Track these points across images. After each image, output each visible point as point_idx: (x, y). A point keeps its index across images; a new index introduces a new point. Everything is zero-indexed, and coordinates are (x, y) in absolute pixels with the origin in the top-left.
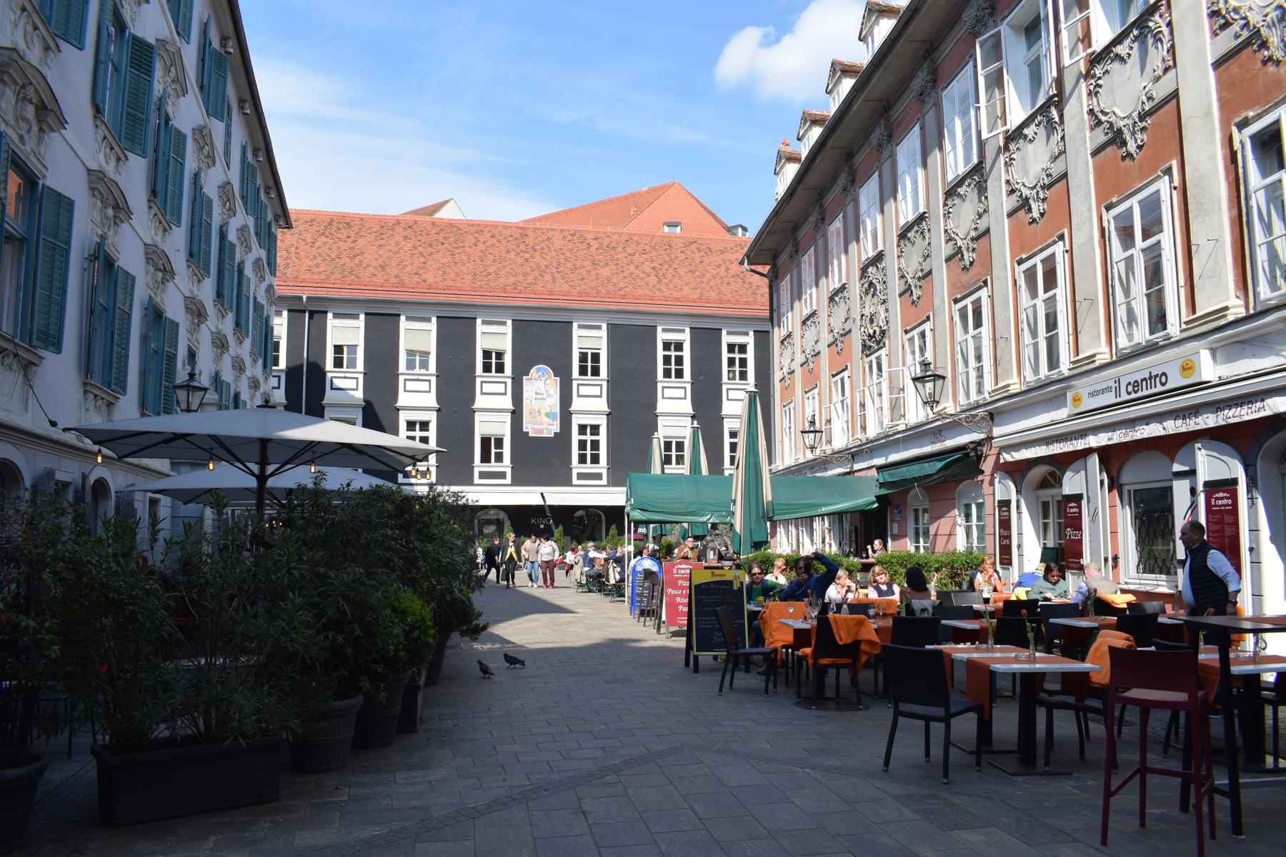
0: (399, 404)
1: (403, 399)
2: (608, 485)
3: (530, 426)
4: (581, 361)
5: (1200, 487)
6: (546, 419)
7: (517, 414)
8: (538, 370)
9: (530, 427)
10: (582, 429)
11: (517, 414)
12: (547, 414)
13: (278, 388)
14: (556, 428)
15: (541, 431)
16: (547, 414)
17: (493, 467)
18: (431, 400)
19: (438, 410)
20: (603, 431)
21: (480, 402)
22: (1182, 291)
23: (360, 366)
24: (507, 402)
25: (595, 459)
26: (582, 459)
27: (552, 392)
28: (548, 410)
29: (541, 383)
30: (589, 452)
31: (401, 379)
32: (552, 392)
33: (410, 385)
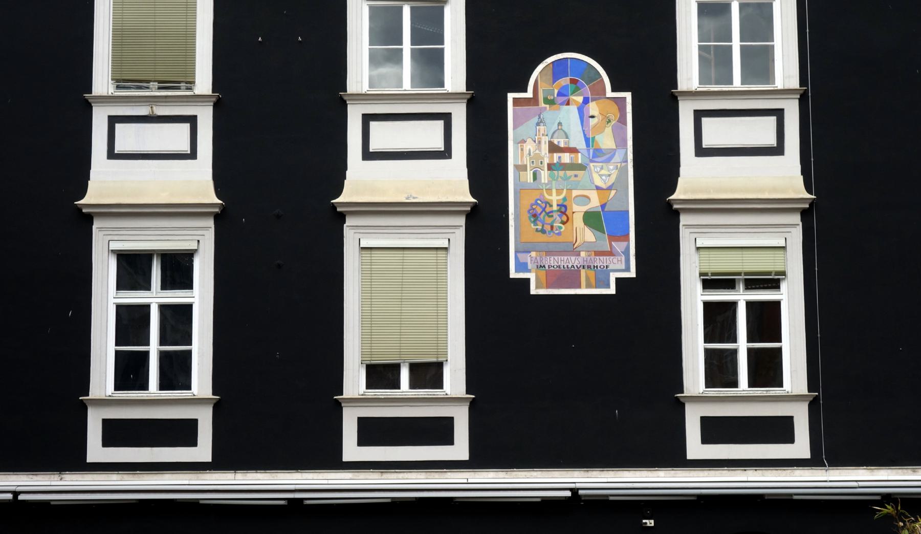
0: (93, 196)
1: (106, 182)
2: (814, 461)
3: (530, 258)
4: (767, 54)
5: (550, 135)
6: (589, 235)
7: (485, 222)
8: (559, 70)
9: (527, 266)
10: (133, 270)
11: (485, 222)
12: (591, 219)
14: (624, 265)
15: (571, 277)
16: (591, 219)
17: (744, 400)
18: (196, 182)
19: (217, 218)
20: (203, 271)
21: (362, 181)
22: (855, 484)
24: (452, 180)
25: (766, 369)
26: (720, 370)
27: (606, 140)
28: (595, 203)
29: (569, 115)
32: (606, 140)
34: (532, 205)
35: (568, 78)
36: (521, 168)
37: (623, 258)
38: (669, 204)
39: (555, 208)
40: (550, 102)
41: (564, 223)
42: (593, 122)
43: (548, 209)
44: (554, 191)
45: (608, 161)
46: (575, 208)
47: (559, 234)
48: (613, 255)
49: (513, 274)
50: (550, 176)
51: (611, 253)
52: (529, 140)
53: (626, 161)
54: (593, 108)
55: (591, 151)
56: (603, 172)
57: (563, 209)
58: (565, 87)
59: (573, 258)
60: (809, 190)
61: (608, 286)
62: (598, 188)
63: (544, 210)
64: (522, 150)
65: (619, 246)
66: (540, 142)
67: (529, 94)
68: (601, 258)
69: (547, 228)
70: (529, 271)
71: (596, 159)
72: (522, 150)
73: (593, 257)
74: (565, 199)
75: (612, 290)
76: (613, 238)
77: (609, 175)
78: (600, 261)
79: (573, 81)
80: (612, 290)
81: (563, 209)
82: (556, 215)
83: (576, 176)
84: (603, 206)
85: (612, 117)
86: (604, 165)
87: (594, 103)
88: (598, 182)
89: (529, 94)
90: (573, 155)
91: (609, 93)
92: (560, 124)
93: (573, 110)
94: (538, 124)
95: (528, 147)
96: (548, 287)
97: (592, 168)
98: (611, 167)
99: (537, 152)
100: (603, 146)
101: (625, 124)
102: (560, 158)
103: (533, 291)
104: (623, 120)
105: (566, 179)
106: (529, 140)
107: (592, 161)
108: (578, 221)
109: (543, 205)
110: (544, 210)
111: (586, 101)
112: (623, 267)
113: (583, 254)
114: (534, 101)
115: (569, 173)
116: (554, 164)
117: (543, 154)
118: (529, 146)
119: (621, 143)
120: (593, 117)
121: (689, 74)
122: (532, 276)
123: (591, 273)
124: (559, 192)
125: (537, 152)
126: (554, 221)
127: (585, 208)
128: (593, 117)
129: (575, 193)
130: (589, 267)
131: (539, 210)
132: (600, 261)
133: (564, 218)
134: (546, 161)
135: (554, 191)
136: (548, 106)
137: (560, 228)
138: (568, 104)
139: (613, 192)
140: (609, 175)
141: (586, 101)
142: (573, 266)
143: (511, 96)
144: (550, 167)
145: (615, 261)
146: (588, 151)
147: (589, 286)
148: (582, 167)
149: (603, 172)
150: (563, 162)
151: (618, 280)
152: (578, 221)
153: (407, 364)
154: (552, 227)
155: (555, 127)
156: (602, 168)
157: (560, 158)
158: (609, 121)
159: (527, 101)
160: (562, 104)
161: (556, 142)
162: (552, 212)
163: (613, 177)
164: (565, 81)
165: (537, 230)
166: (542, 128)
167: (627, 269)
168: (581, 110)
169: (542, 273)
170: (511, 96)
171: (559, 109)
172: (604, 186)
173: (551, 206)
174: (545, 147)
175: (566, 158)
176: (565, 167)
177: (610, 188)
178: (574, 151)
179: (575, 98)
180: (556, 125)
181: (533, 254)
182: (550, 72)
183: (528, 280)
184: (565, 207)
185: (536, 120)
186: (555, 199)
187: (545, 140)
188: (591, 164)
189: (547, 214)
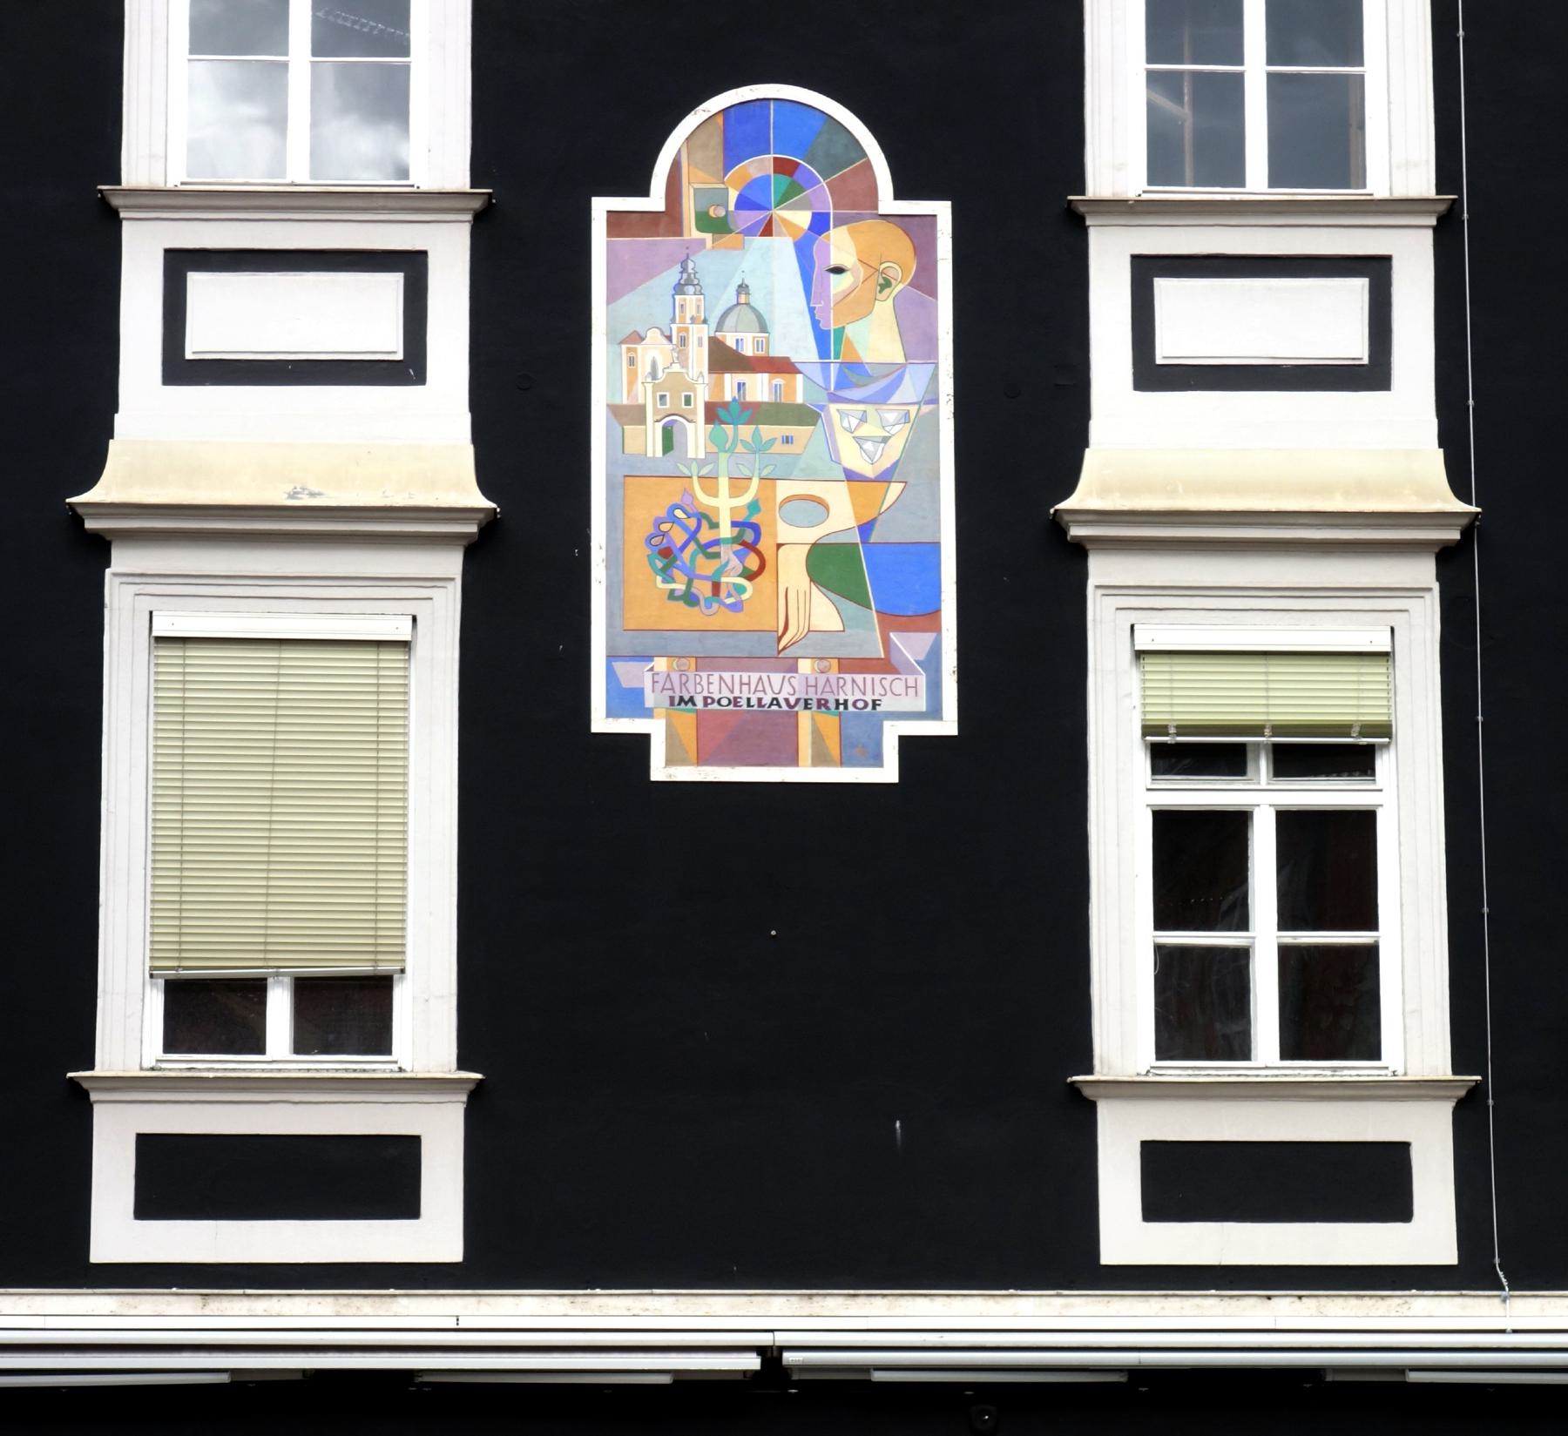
8: (741, 135)
9: (646, 696)
12: (831, 566)
13: (409, 368)
14: (921, 697)
15: (769, 731)
16: (831, 566)
17: (1269, 1098)
21: (160, 441)
23: (1400, 142)
24: (426, 445)
25: (1332, 1010)
26: (1198, 1008)
27: (876, 338)
28: (841, 520)
29: (770, 265)
30: (1264, 937)
31: (1108, 261)
32: (876, 338)
33: (1195, 320)
38: (1057, 527)
60: (1460, 490)
121: (1115, 156)
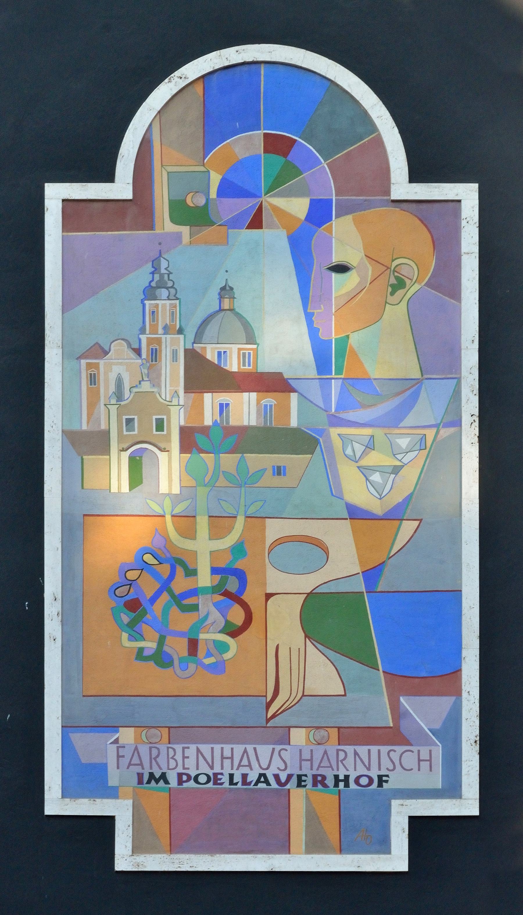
3: (118, 749)
5: (191, 337)
6: (322, 674)
8: (225, 106)
12: (328, 617)
15: (258, 812)
16: (328, 617)
27: (385, 351)
28: (343, 563)
34: (124, 571)
35: (260, 133)
36: (88, 443)
37: (438, 752)
39: (205, 579)
40: (195, 217)
41: (235, 632)
42: (342, 285)
43: (180, 584)
44: (203, 524)
45: (393, 420)
46: (275, 580)
47: (218, 668)
48: (404, 741)
49: (56, 803)
50: (187, 469)
51: (393, 735)
52: (119, 349)
53: (457, 423)
54: (344, 239)
55: (335, 387)
56: (374, 459)
57: (233, 585)
58: (250, 165)
59: (265, 750)
61: (383, 846)
62: (355, 514)
63: (166, 586)
64: (93, 379)
65: (423, 712)
66: (155, 355)
67: (121, 187)
68: (362, 750)
69: (178, 647)
70: (112, 793)
71: (351, 415)
72: (93, 379)
73: (332, 748)
74: (238, 549)
75: (397, 859)
76: (401, 683)
77: (396, 470)
78: (357, 762)
79: (276, 145)
80: (397, 859)
81: (233, 585)
82: (207, 605)
83: (279, 471)
84: (372, 575)
85: (409, 268)
86: (379, 433)
87: (348, 219)
88: (357, 492)
89: (121, 187)
90: (270, 400)
91: (402, 187)
92: (226, 291)
93: (274, 239)
94: (150, 293)
95: (116, 370)
96: (174, 848)
97: (337, 442)
98: (404, 442)
99: (146, 386)
100: (375, 371)
101: (455, 293)
102: (223, 407)
103: (125, 859)
104: (445, 281)
105: (243, 480)
106: (119, 349)
107: (336, 421)
108: (284, 625)
109: (165, 570)
110: (166, 586)
111: (320, 213)
112: (437, 781)
113: (298, 737)
114: (138, 210)
115: (256, 461)
116: (205, 431)
117: (165, 392)
118: (119, 367)
119: (438, 360)
120: (341, 269)
122: (120, 811)
123: (326, 801)
124: (219, 524)
125: (146, 386)
126: (201, 625)
127: (308, 583)
128: (341, 269)
129: (274, 529)
130: (319, 781)
131: (148, 586)
132: (357, 762)
133: (237, 615)
134: (177, 419)
135: (203, 524)
136: (185, 230)
137: (223, 647)
138: (256, 222)
139: (408, 528)
140: (396, 470)
141: (320, 213)
142: (263, 778)
143: (56, 194)
144: (189, 440)
145: (410, 760)
146: (325, 384)
147: (316, 845)
148: (302, 442)
149: (374, 459)
150: (233, 422)
151: (417, 824)
152: (284, 625)
153: (183, 243)
154: (193, 645)
155: (211, 301)
156: (370, 446)
157: (223, 407)
158: (400, 284)
159: (112, 213)
160: (234, 223)
161: (211, 355)
162: (194, 592)
163: (410, 477)
164: (247, 144)
165: (140, 654)
166: (163, 304)
167: (452, 789)
168: (302, 247)
169: (158, 797)
170: (56, 194)
171: (225, 241)
172: (376, 507)
173: (192, 573)
174: (173, 373)
175: (246, 409)
176: (243, 440)
177: (395, 515)
178: (274, 384)
179: (280, 202)
180: (214, 293)
181: (127, 736)
182: (195, 113)
183: (107, 823)
184: (240, 575)
185: (142, 277)
186: (205, 549)
187: (172, 348)
188: (334, 432)
189: (179, 599)
